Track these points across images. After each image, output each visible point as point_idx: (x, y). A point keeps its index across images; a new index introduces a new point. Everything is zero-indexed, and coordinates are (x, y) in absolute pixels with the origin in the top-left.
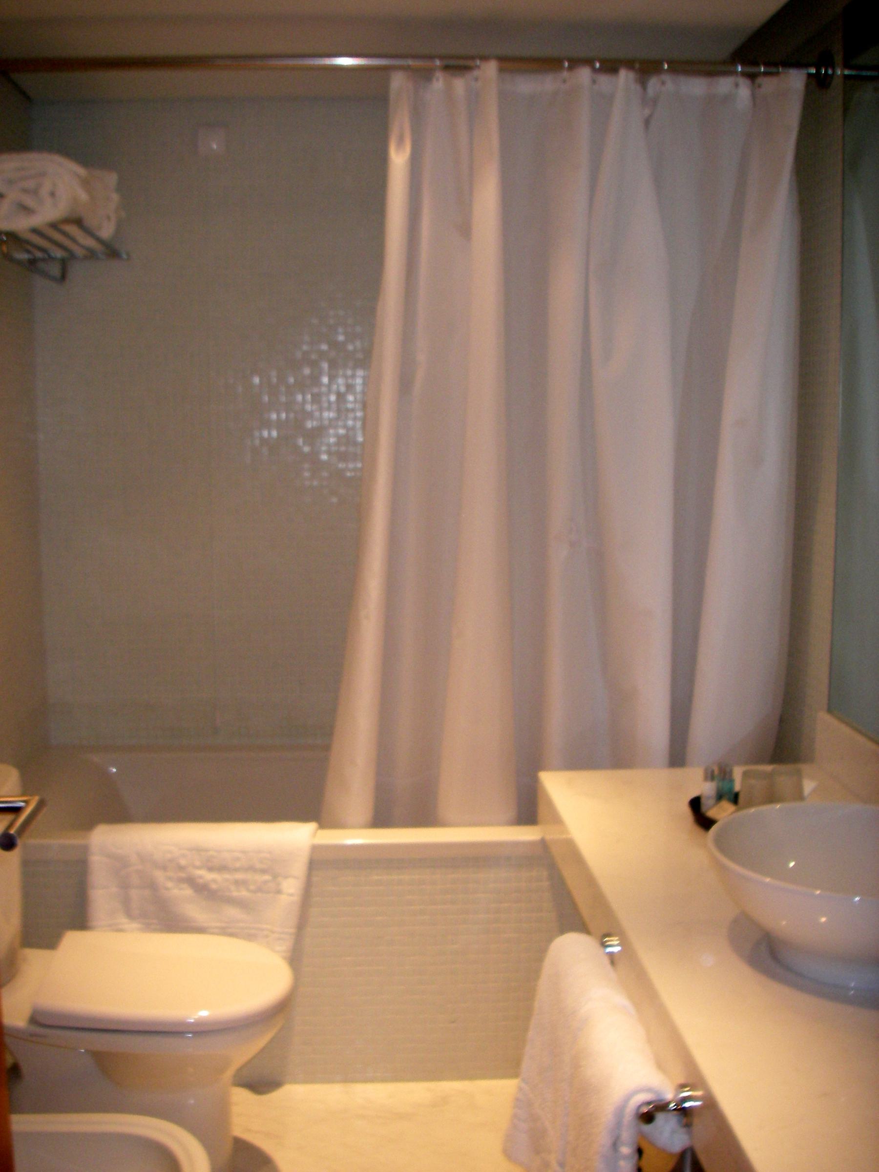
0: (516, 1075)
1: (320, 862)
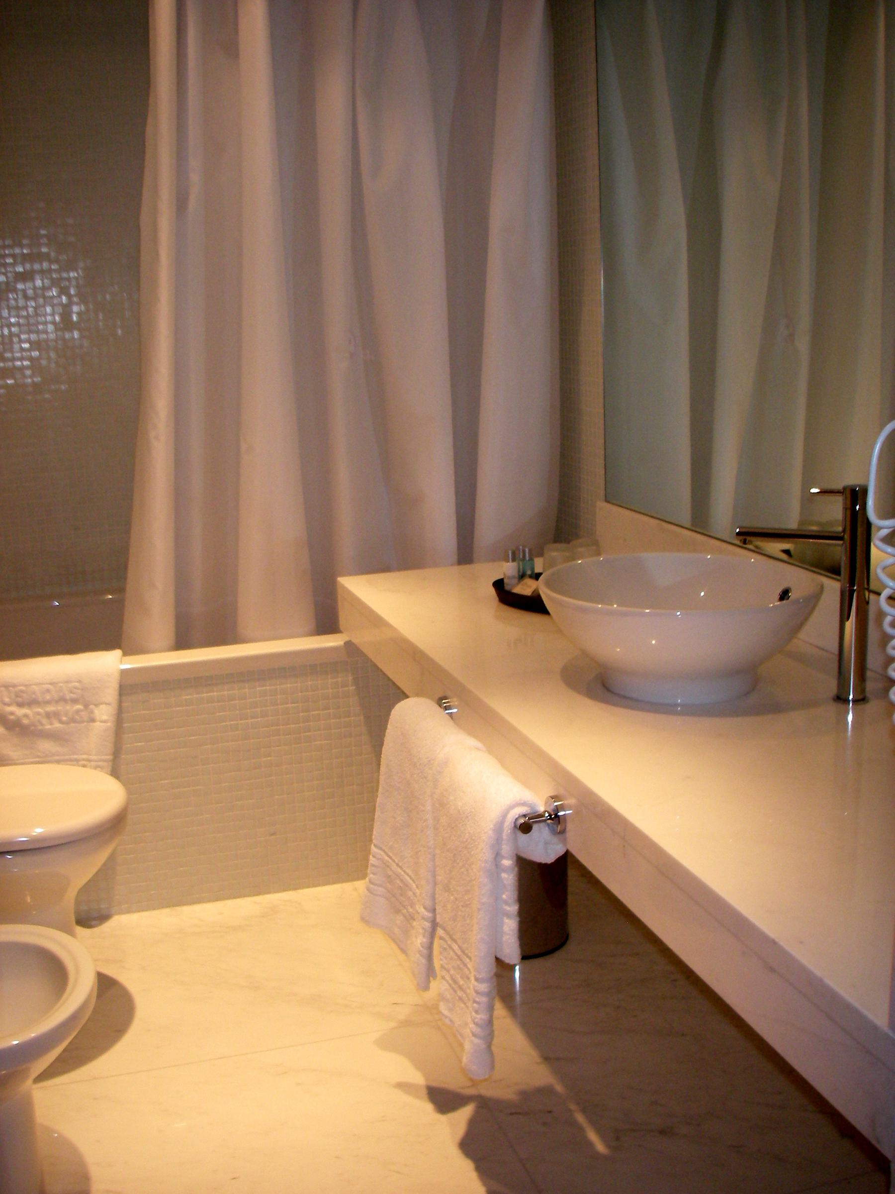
0: (352, 866)
1: (129, 686)
